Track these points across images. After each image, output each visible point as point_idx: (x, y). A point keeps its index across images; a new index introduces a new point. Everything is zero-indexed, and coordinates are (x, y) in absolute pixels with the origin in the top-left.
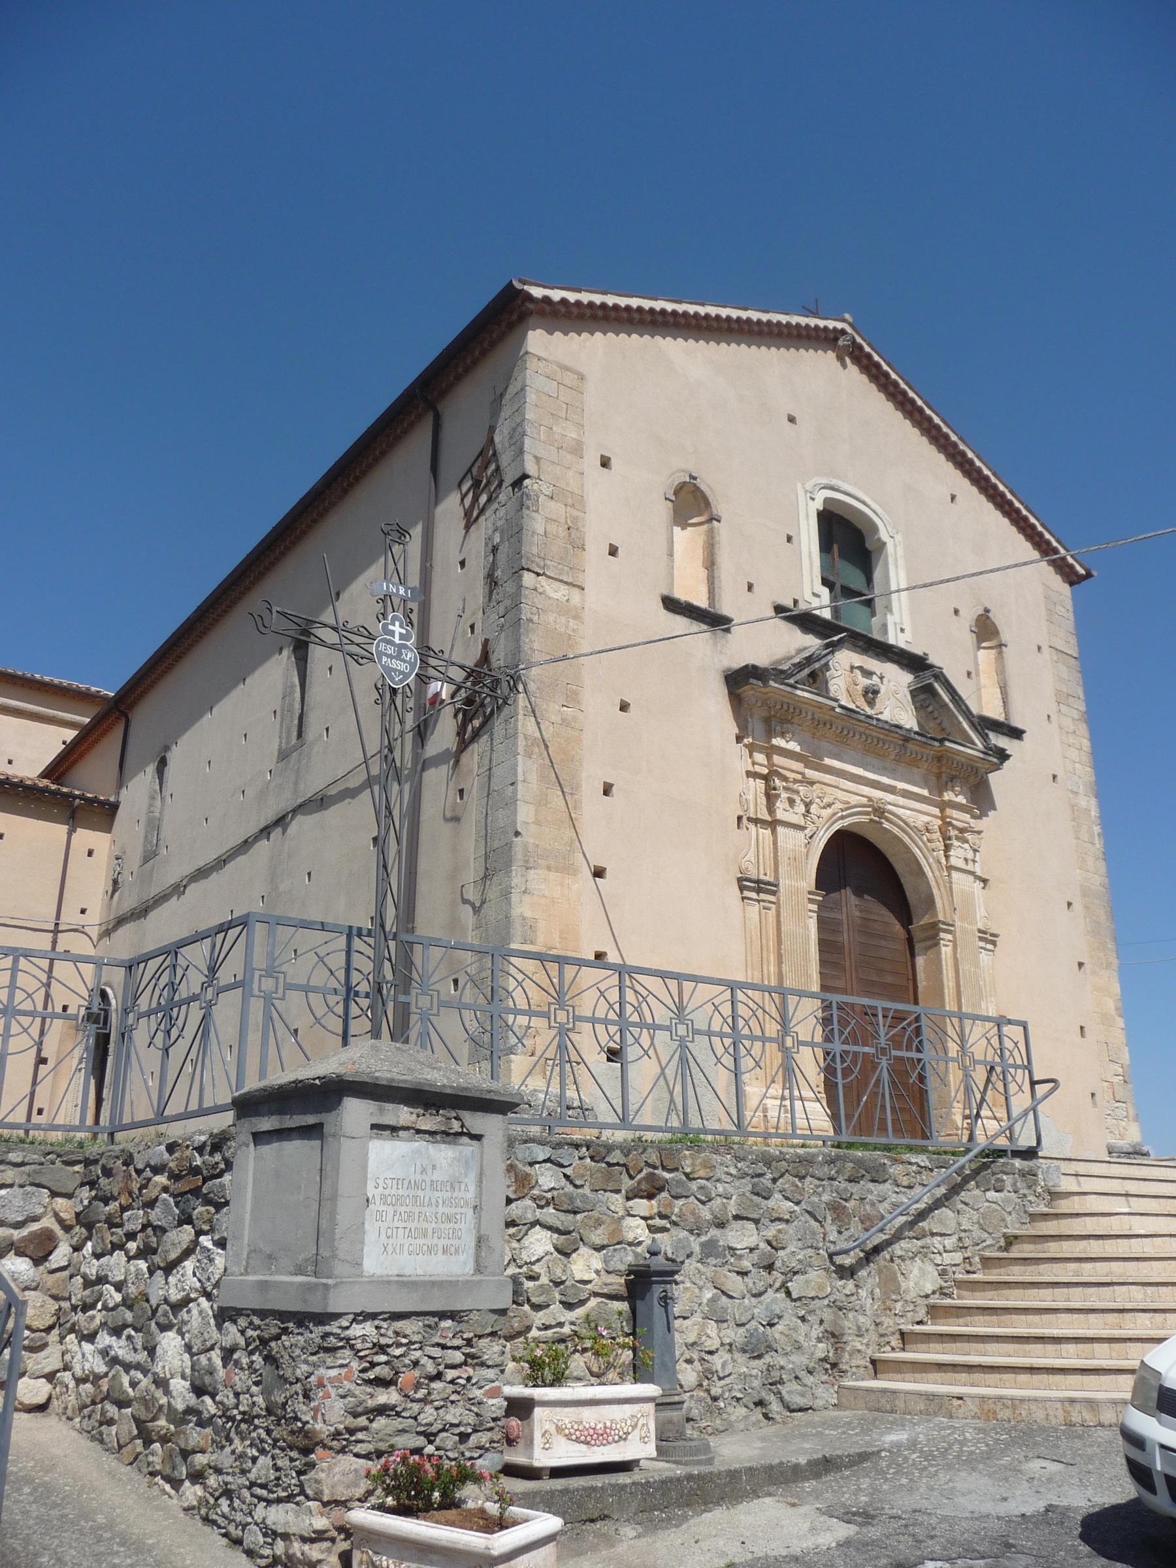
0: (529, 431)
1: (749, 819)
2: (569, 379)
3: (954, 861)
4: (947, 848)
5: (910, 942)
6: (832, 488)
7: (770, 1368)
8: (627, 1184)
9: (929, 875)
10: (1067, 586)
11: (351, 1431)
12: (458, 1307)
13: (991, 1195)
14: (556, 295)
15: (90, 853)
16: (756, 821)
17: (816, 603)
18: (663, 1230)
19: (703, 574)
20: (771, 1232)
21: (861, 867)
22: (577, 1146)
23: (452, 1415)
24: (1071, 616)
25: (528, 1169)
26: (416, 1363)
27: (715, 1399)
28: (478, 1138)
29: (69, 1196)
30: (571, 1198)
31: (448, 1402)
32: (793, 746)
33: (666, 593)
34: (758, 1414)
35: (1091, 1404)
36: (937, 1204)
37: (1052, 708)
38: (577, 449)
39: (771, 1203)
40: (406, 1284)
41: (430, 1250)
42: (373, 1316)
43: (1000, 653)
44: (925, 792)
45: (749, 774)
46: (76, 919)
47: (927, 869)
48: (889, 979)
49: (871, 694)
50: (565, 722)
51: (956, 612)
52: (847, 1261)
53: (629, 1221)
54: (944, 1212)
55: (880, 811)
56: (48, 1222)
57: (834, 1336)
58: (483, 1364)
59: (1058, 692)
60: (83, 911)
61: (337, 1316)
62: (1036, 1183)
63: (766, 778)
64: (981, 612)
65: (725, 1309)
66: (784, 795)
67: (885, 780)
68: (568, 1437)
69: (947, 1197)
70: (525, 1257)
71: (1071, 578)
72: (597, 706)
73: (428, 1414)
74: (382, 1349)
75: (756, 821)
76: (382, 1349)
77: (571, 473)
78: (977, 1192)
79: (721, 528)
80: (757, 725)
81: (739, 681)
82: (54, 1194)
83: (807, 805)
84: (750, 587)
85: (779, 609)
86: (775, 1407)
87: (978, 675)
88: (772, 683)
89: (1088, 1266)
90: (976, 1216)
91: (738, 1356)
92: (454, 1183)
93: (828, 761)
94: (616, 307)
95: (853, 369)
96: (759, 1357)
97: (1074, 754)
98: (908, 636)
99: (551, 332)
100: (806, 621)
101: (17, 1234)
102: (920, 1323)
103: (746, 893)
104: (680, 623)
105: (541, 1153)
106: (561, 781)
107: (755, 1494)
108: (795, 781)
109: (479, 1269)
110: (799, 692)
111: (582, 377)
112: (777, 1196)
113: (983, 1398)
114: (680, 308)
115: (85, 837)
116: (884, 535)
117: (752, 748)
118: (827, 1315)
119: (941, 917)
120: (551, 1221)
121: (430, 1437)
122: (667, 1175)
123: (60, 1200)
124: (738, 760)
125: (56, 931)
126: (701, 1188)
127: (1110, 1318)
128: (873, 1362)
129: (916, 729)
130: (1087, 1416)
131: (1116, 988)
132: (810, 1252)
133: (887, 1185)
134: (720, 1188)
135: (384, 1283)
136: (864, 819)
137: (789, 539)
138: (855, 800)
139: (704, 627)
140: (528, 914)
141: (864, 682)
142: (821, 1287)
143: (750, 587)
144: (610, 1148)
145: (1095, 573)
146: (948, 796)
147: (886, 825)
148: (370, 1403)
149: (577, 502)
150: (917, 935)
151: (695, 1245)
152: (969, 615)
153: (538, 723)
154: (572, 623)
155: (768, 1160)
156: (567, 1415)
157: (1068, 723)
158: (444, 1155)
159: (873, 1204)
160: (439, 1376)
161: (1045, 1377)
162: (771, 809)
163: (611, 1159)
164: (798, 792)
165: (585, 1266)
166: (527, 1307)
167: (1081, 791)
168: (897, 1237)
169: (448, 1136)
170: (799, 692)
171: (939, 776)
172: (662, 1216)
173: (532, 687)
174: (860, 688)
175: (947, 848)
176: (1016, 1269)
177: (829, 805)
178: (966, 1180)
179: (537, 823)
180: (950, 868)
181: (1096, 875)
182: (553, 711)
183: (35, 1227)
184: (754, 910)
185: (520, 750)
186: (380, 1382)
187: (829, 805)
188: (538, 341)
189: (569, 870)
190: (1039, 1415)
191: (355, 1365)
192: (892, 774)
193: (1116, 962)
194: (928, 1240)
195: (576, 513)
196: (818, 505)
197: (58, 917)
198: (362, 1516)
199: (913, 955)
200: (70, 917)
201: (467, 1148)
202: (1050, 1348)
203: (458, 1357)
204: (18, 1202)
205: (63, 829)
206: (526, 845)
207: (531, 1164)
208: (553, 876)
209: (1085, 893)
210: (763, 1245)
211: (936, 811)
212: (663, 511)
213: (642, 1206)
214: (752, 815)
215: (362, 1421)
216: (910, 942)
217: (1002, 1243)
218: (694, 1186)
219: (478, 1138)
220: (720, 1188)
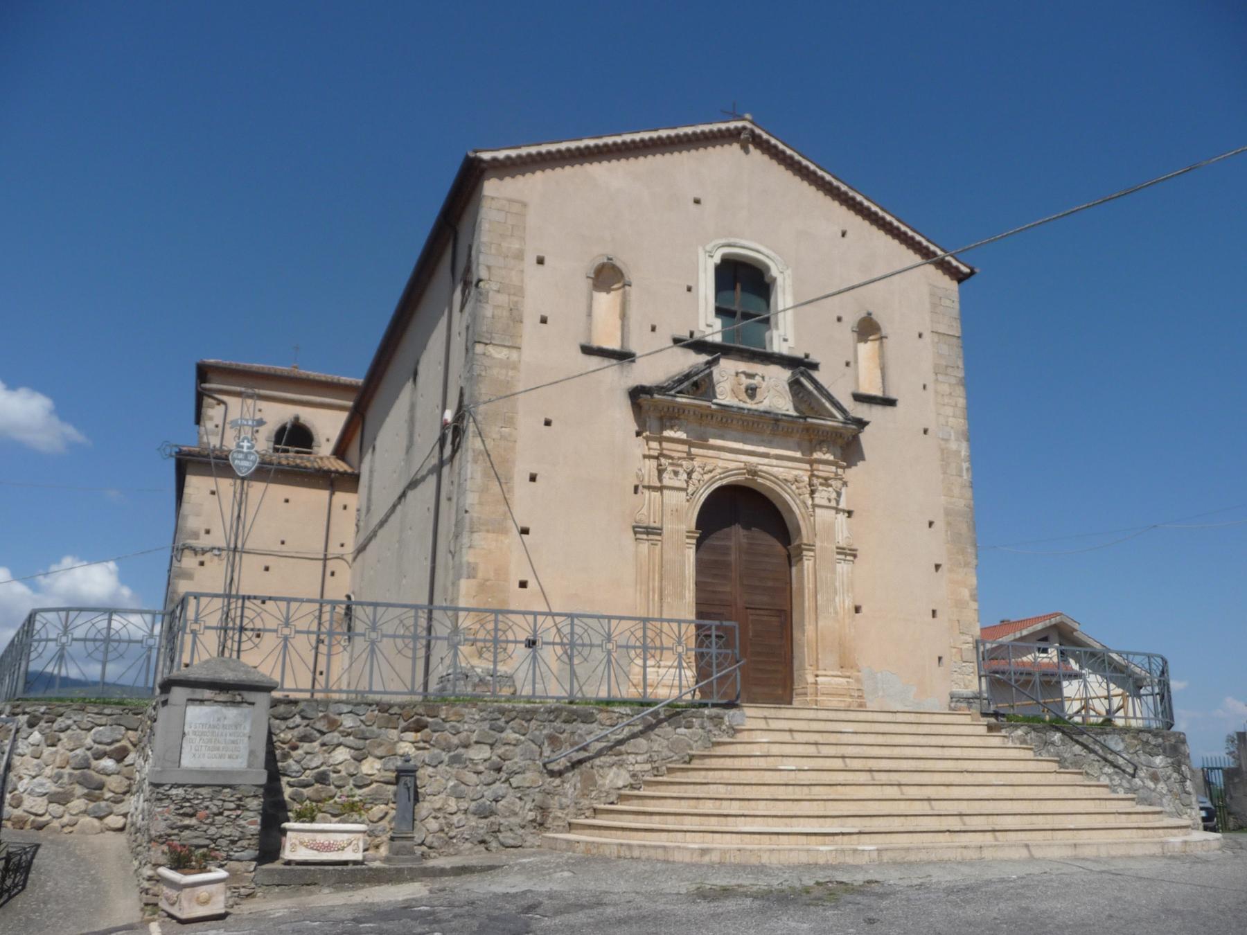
0: (483, 249)
1: (644, 487)
2: (516, 208)
3: (817, 501)
4: (812, 492)
5: (789, 557)
6: (729, 245)
7: (492, 823)
8: (403, 724)
9: (797, 511)
10: (955, 283)
11: (169, 835)
12: (232, 782)
13: (682, 730)
14: (501, 155)
15: (345, 507)
16: (649, 488)
17: (709, 331)
18: (424, 749)
19: (619, 323)
20: (500, 751)
21: (741, 513)
22: (370, 705)
23: (226, 832)
24: (957, 306)
25: (337, 717)
26: (207, 808)
27: (451, 838)
28: (253, 704)
29: (136, 730)
30: (363, 732)
31: (223, 826)
32: (682, 435)
33: (584, 341)
34: (482, 847)
35: (630, 846)
36: (634, 736)
37: (930, 379)
38: (520, 256)
39: (503, 735)
40: (203, 772)
41: (221, 757)
42: (183, 786)
43: (881, 343)
44: (798, 455)
45: (645, 457)
46: (339, 551)
47: (795, 508)
48: (770, 584)
49: (752, 392)
50: (502, 437)
51: (839, 319)
52: (554, 767)
53: (402, 744)
54: (642, 741)
55: (754, 473)
56: (124, 743)
57: (543, 809)
58: (248, 810)
59: (936, 366)
60: (342, 545)
61: (163, 785)
62: (722, 723)
63: (657, 458)
64: (863, 314)
65: (462, 792)
66: (670, 469)
67: (762, 449)
68: (306, 846)
69: (642, 733)
70: (331, 761)
71: (960, 277)
72: (527, 424)
73: (212, 830)
74: (188, 800)
75: (649, 488)
76: (188, 800)
77: (513, 273)
78: (669, 729)
79: (633, 292)
80: (653, 423)
81: (637, 395)
82: (128, 729)
83: (689, 474)
84: (653, 329)
85: (677, 341)
86: (494, 844)
87: (856, 362)
88: (656, 396)
89: (711, 773)
90: (665, 743)
91: (469, 816)
92: (237, 726)
93: (712, 441)
94: (549, 153)
95: (755, 153)
96: (485, 817)
97: (949, 411)
98: (791, 343)
99: (501, 178)
100: (699, 346)
101: (108, 748)
102: (612, 803)
103: (639, 536)
104: (595, 362)
105: (346, 709)
106: (498, 474)
107: (412, 880)
108: (679, 458)
109: (249, 766)
110: (679, 399)
111: (525, 205)
112: (509, 731)
113: (587, 843)
114: (600, 142)
115: (341, 497)
116: (774, 272)
117: (648, 439)
118: (538, 797)
119: (805, 541)
120: (348, 743)
121: (214, 840)
122: (430, 720)
123: (130, 732)
124: (638, 447)
125: (325, 559)
126: (453, 727)
127: (692, 802)
128: (570, 824)
129: (792, 412)
130: (627, 853)
131: (973, 581)
132: (528, 762)
133: (594, 725)
134: (466, 727)
135: (190, 771)
136: (740, 478)
137: (689, 289)
138: (732, 465)
139: (615, 362)
140: (472, 560)
141: (746, 381)
142: (533, 781)
143: (653, 329)
144: (391, 706)
145: (977, 270)
146: (817, 455)
147: (760, 480)
148: (179, 824)
149: (520, 291)
150: (793, 553)
151: (445, 757)
152: (851, 319)
153: (483, 441)
154: (511, 373)
155: (502, 712)
156: (307, 837)
157: (945, 388)
158: (231, 713)
159: (580, 736)
160: (221, 814)
161: (613, 832)
162: (660, 479)
163: (392, 711)
164: (681, 466)
165: (370, 767)
166: (332, 787)
167: (953, 437)
168: (599, 754)
169: (233, 703)
170: (679, 399)
171: (811, 441)
172: (425, 742)
173: (479, 418)
174: (743, 388)
175: (812, 492)
176: (679, 774)
177: (711, 471)
178: (660, 722)
179: (481, 504)
180: (814, 506)
181: (961, 499)
182: (493, 431)
183: (118, 745)
184: (644, 547)
185: (470, 459)
186: (185, 815)
187: (711, 471)
188: (491, 187)
189: (504, 531)
190: (607, 853)
191: (172, 807)
192: (770, 444)
193: (974, 562)
194: (624, 757)
195: (516, 299)
196: (717, 259)
197: (326, 549)
198: (165, 872)
199: (790, 566)
200: (334, 549)
201: (246, 709)
202: (648, 818)
203: (232, 806)
204: (108, 733)
205: (325, 494)
206: (471, 519)
207: (340, 714)
208: (490, 535)
209: (948, 513)
210: (494, 758)
211: (807, 466)
212: (584, 285)
213: (411, 736)
214: (646, 484)
215: (176, 831)
216: (789, 557)
217: (687, 759)
218: (447, 725)
219: (253, 704)
220: (466, 727)
